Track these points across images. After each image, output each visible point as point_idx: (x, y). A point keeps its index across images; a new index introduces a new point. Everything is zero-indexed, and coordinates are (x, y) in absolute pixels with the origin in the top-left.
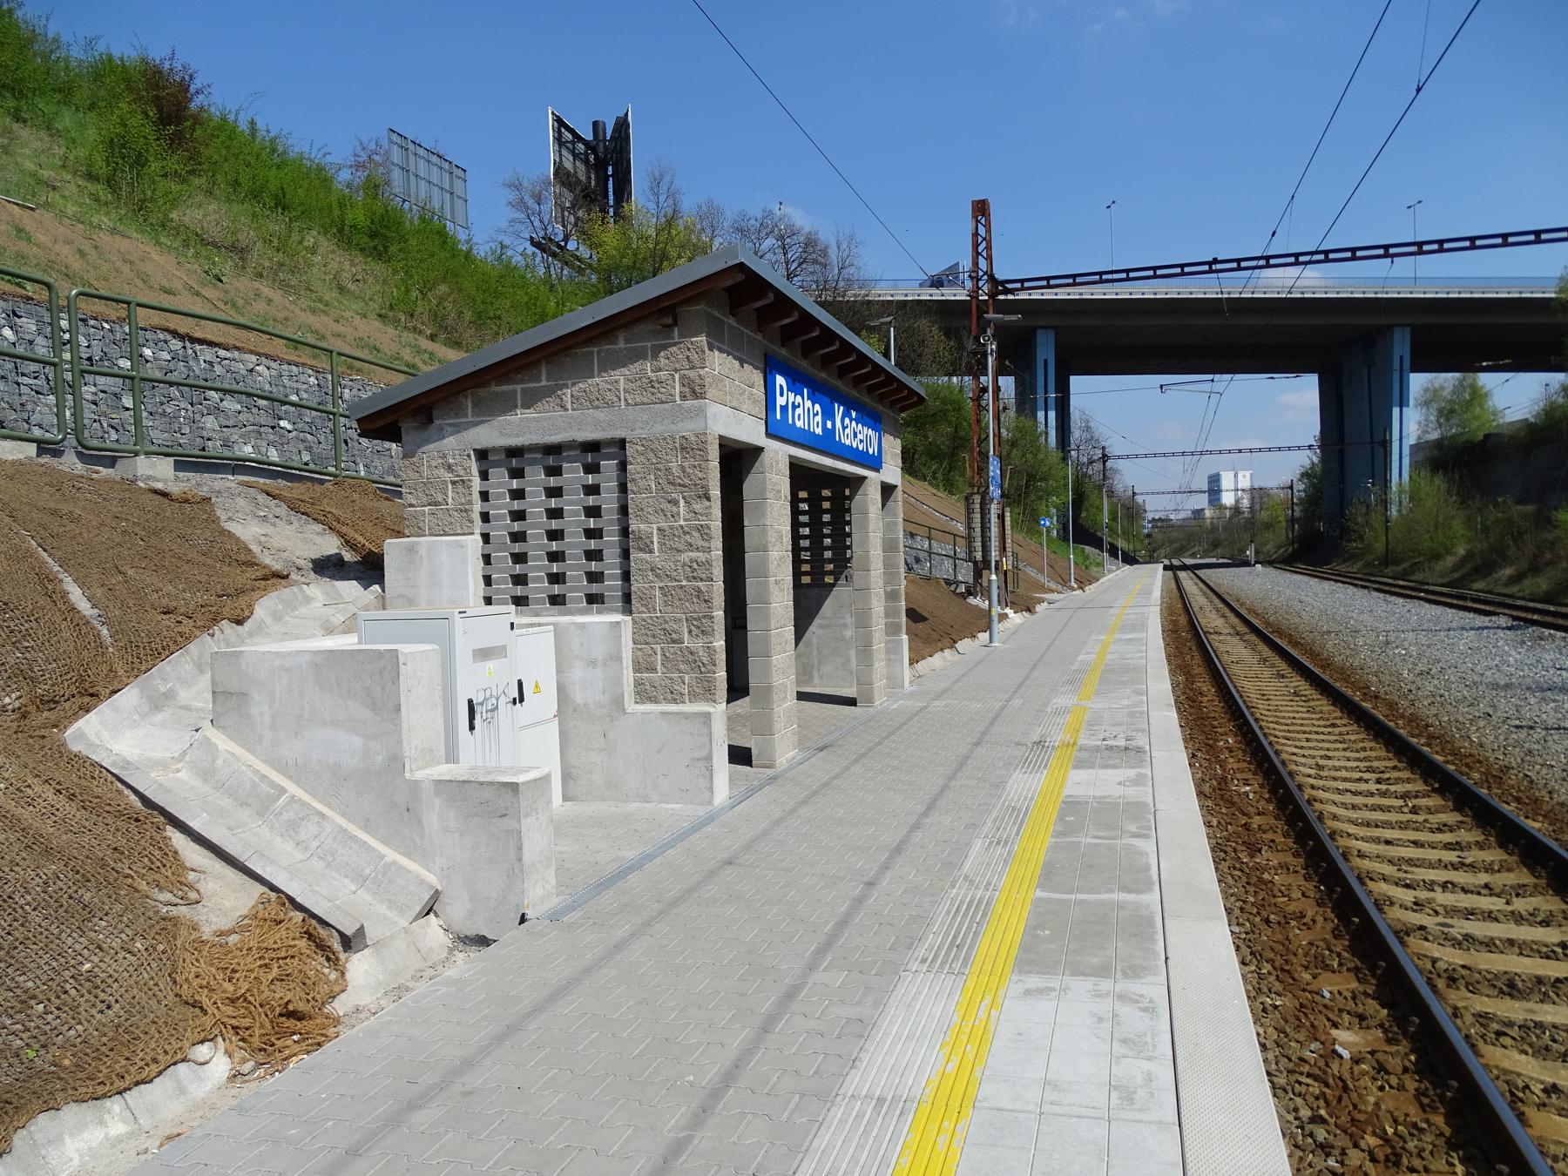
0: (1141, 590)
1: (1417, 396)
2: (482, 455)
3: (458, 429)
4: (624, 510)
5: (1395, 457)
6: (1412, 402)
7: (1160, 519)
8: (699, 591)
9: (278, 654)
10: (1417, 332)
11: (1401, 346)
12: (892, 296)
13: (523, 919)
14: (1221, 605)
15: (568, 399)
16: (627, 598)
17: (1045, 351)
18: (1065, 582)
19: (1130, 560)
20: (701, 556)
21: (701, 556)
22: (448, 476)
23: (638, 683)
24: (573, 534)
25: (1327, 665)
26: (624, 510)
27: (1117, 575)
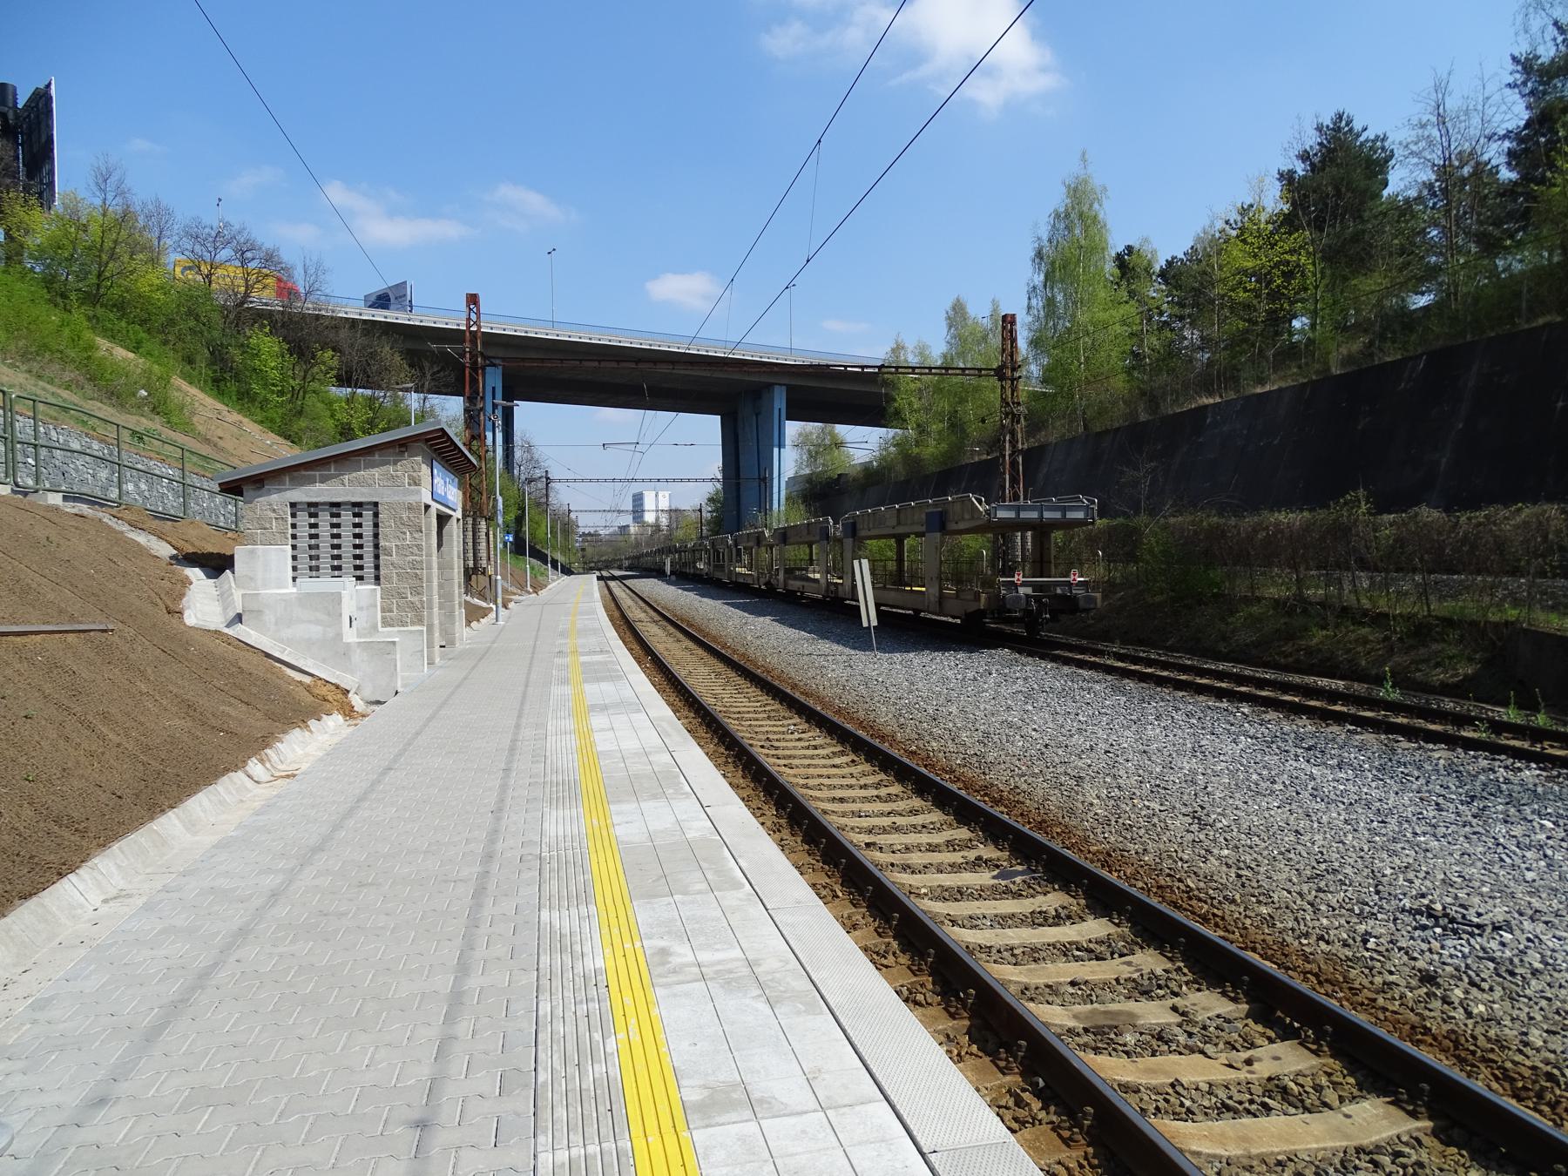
1: (794, 438)
2: (293, 505)
3: (280, 491)
4: (376, 536)
5: (775, 490)
6: (788, 441)
7: (589, 534)
8: (416, 574)
9: (279, 594)
10: (790, 390)
11: (779, 401)
12: (346, 313)
13: (397, 693)
14: (643, 605)
15: (346, 482)
16: (377, 578)
17: (493, 379)
18: (522, 587)
19: (567, 571)
20: (418, 558)
21: (418, 558)
22: (273, 515)
23: (383, 618)
24: (345, 546)
25: (707, 635)
26: (376, 536)
27: (558, 583)
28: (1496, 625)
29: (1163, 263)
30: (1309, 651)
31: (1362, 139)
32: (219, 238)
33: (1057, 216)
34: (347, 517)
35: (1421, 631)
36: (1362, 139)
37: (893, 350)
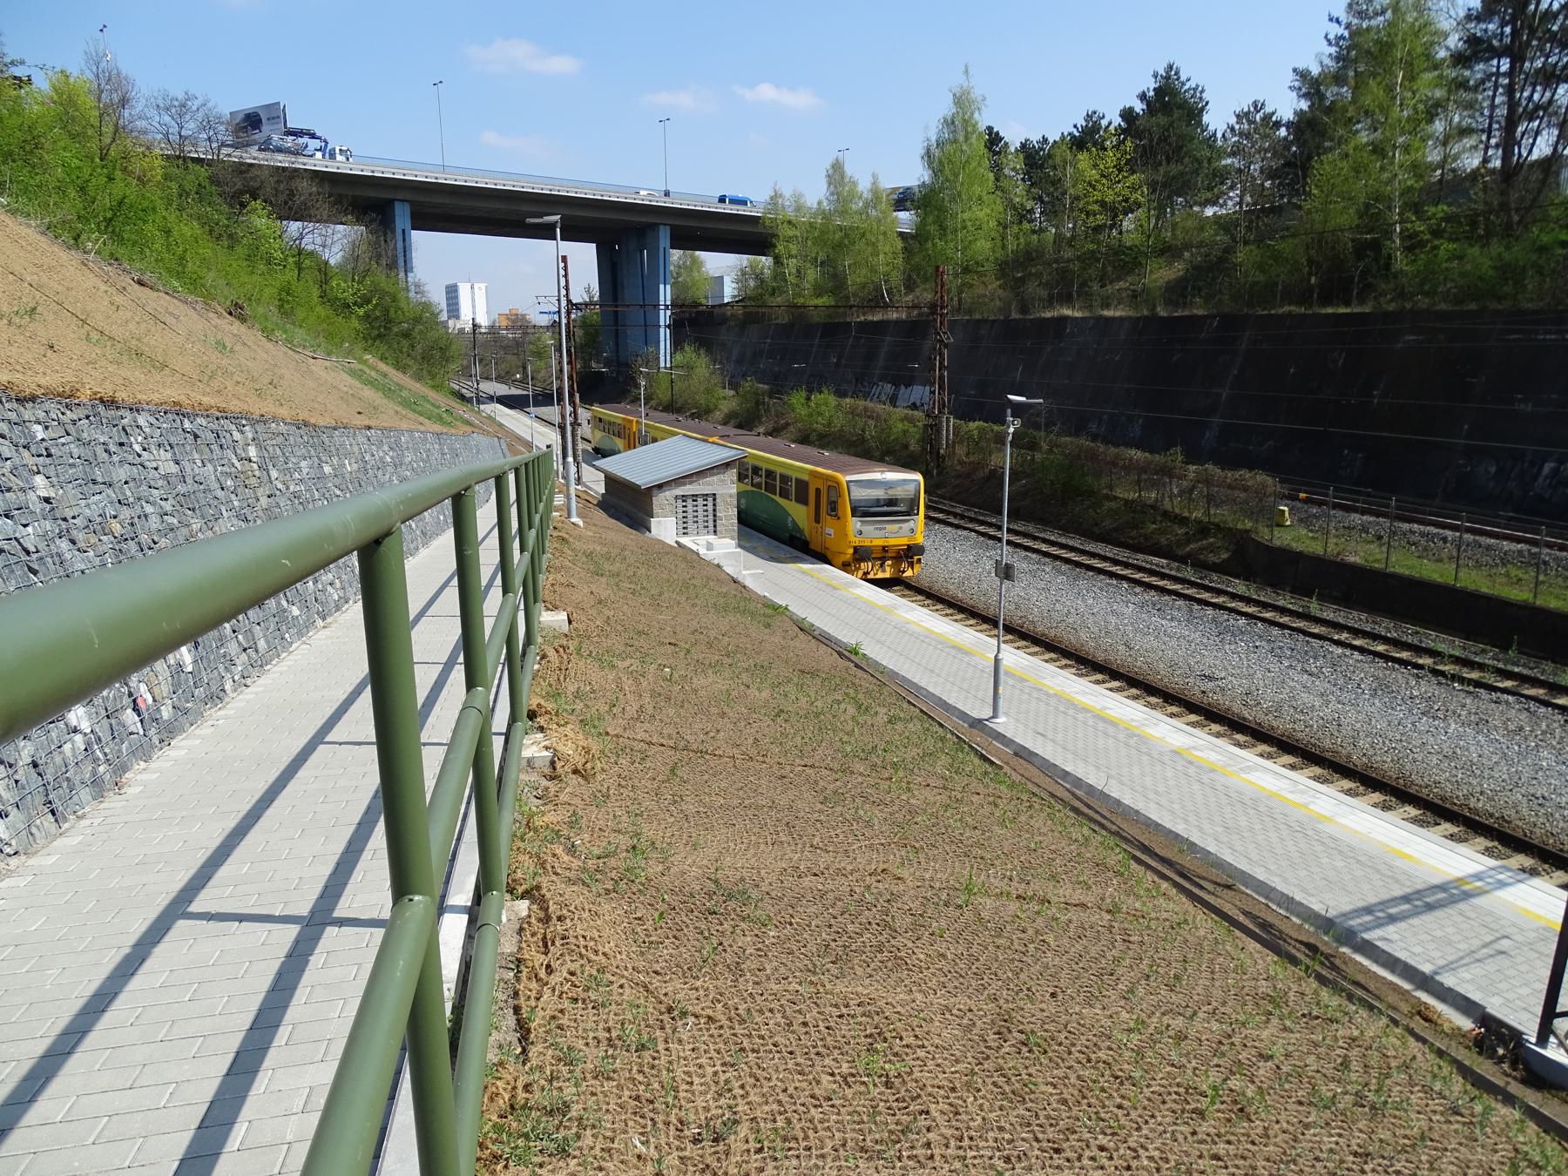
28: (1240, 531)
29: (1018, 145)
30: (1146, 537)
31: (1186, 87)
33: (945, 120)
34: (700, 501)
35: (1203, 530)
36: (1186, 87)
37: (772, 198)
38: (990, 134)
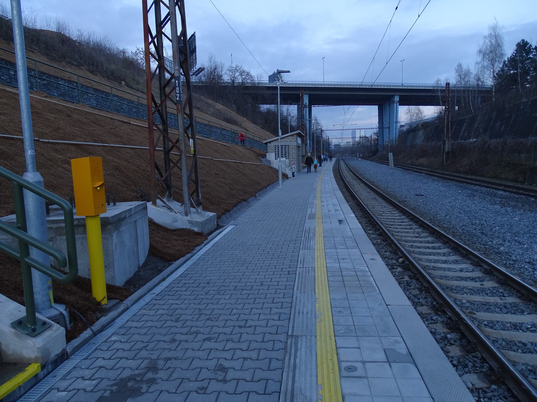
0: (418, 232)
17: (306, 100)
32: (236, 70)
38: (523, 43)
